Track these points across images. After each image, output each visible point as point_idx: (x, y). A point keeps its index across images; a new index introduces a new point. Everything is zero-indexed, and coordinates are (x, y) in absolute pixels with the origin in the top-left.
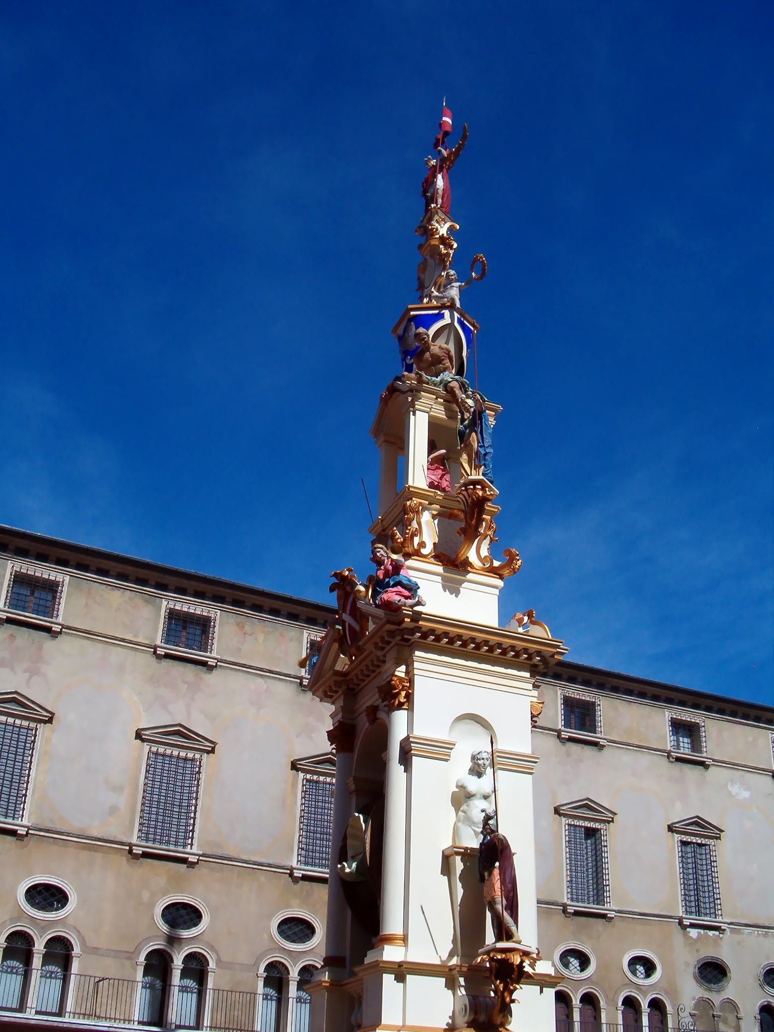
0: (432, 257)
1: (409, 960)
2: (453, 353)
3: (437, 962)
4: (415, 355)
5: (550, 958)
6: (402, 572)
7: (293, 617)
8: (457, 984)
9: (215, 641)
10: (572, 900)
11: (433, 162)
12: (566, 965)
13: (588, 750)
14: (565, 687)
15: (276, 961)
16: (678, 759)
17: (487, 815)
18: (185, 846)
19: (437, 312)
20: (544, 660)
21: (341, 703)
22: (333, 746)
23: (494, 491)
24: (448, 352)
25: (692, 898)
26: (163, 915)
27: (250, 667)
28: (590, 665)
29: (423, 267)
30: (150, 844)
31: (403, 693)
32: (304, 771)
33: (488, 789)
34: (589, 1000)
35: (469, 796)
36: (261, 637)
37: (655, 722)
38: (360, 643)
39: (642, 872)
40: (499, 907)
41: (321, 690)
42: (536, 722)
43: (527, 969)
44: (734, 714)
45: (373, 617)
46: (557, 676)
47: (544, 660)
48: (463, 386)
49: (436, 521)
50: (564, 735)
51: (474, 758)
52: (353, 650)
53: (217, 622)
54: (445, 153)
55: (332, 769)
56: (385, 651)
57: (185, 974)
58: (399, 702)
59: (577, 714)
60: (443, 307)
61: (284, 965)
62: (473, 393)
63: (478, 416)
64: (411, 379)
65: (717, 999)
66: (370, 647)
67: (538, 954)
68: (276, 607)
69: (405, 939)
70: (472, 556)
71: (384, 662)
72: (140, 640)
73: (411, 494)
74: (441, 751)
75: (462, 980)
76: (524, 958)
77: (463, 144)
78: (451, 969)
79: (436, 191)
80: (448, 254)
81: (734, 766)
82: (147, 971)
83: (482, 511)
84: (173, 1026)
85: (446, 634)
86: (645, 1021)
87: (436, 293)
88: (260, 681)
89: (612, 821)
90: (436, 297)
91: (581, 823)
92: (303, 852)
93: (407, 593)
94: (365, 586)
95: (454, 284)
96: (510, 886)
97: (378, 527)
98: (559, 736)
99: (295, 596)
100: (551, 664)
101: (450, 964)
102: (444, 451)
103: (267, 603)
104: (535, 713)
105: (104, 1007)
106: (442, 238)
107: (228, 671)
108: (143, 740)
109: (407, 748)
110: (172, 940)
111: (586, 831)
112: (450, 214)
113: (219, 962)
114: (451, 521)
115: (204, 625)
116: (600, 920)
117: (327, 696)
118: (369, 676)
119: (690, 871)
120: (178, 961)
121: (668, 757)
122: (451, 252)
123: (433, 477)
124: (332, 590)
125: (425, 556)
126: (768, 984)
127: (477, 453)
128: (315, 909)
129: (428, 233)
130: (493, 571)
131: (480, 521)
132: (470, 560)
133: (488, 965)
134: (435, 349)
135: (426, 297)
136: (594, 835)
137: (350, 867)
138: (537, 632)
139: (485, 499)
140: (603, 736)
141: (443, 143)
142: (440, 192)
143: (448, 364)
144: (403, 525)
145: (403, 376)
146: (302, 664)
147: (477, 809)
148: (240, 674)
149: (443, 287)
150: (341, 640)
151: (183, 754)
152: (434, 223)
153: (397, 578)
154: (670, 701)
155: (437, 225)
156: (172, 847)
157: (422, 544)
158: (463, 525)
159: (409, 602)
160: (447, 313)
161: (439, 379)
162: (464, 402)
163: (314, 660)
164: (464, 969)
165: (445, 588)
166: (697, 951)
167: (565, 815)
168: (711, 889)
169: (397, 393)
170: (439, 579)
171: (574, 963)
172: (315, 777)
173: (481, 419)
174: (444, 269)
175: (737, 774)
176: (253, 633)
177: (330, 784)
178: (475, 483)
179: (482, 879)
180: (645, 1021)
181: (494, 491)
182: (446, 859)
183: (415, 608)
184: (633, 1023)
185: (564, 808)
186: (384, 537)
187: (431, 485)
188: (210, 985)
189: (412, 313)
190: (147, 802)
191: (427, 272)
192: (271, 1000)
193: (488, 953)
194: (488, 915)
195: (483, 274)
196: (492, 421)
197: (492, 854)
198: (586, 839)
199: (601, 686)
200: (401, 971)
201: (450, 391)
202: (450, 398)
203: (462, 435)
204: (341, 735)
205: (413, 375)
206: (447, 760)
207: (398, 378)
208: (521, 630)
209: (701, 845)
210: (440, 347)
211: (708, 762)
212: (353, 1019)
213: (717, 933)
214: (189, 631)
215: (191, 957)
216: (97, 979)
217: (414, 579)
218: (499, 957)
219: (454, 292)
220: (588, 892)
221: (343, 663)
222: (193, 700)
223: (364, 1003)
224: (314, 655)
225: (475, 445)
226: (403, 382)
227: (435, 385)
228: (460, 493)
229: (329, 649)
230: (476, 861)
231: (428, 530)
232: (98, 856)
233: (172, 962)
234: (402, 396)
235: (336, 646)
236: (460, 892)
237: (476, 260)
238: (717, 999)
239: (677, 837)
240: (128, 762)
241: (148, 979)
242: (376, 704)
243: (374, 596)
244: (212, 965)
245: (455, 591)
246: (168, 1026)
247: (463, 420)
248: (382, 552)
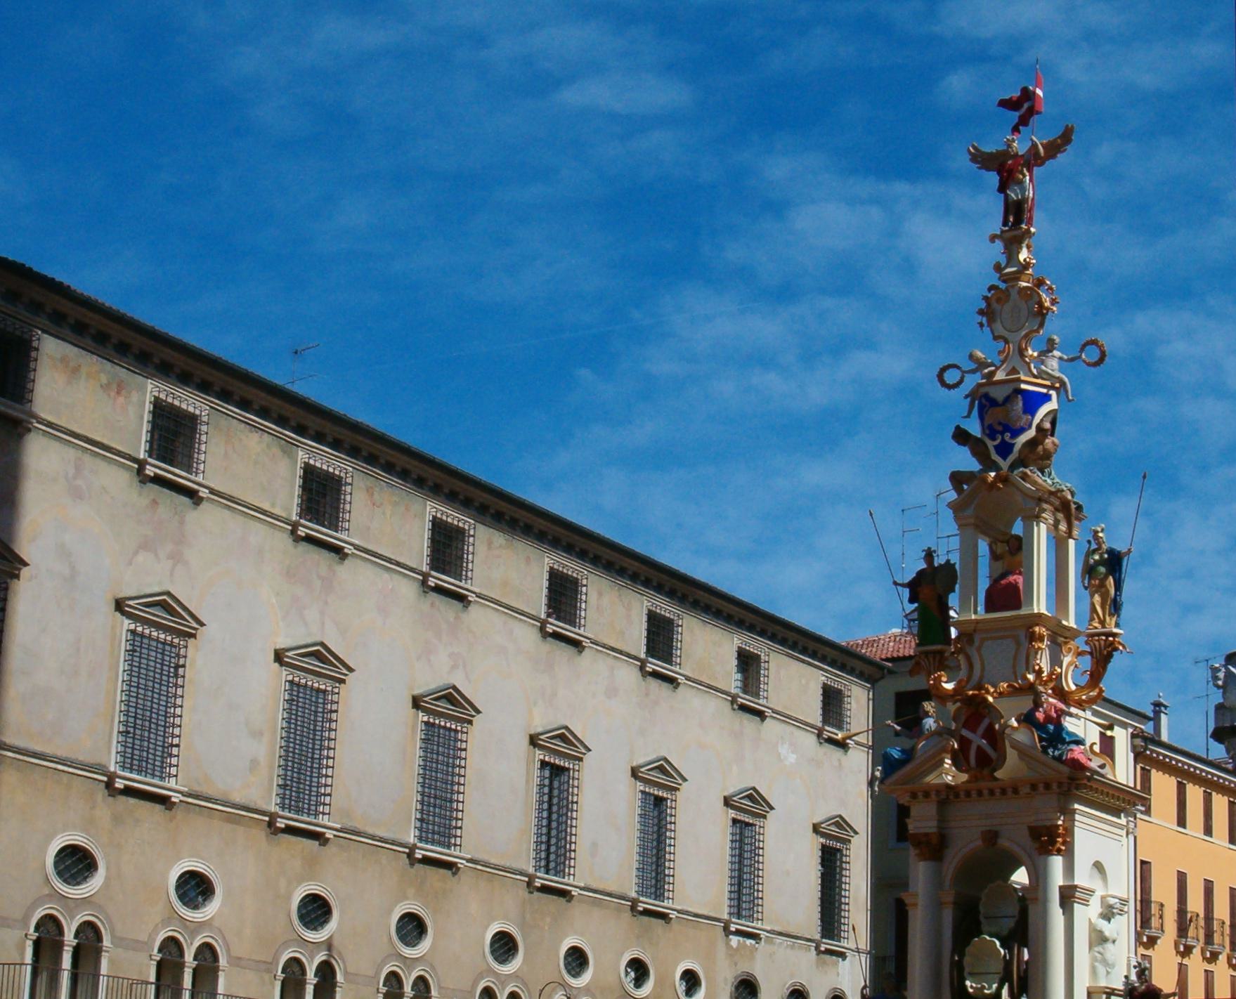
19: (1044, 391)
28: (244, 366)
72: (277, 511)
89: (194, 636)
121: (733, 702)
148: (369, 565)
167: (130, 616)
185: (131, 603)
209: (748, 824)
213: (753, 942)
222: (326, 603)
239: (732, 814)
240: (265, 690)
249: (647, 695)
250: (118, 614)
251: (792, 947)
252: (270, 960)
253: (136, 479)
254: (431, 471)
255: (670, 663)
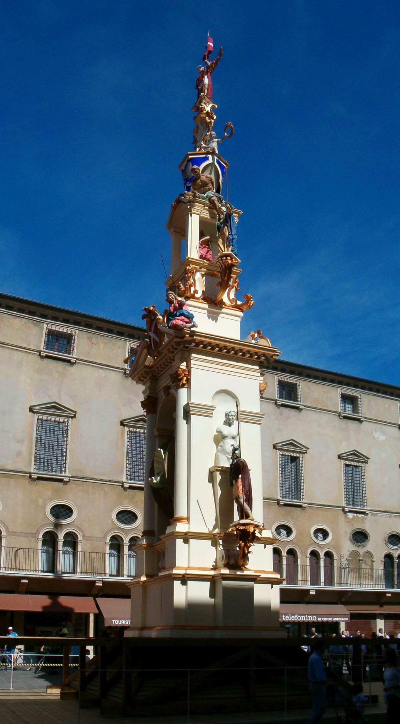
0: (201, 124)
1: (191, 531)
2: (214, 180)
3: (207, 531)
4: (192, 181)
5: (270, 529)
6: (184, 308)
7: (120, 334)
8: (218, 544)
9: (75, 348)
10: (283, 497)
11: (202, 69)
12: (279, 534)
13: (293, 412)
14: (279, 374)
15: (116, 535)
16: (345, 417)
17: (234, 448)
18: (61, 472)
19: (204, 156)
20: (267, 359)
21: (148, 384)
22: (145, 410)
23: (238, 260)
24: (211, 180)
25: (351, 496)
26: (51, 512)
27: (95, 363)
29: (197, 128)
30: (41, 472)
31: (185, 378)
32: (128, 426)
33: (235, 433)
34: (292, 552)
35: (224, 437)
36: (102, 346)
37: (332, 395)
38: (160, 349)
39: (322, 481)
40: (241, 500)
41: (137, 376)
42: (262, 394)
43: (257, 534)
44: (378, 391)
45: (167, 334)
46: (275, 369)
47: (267, 359)
48: (220, 200)
49: (204, 278)
50: (279, 403)
51: (227, 415)
52: (156, 353)
53: (76, 337)
54: (209, 63)
55: (145, 425)
56: (174, 354)
57: (65, 544)
58: (183, 383)
59: (286, 390)
60: (208, 153)
61: (120, 537)
62: (226, 203)
63: (229, 217)
64: (189, 195)
65: (362, 551)
66: (165, 351)
67: (263, 526)
68: (110, 328)
69: (188, 519)
70: (225, 298)
71: (174, 360)
72: (31, 347)
73: (189, 262)
74: (207, 411)
75: (221, 542)
76: (256, 528)
77: (220, 58)
78: (215, 535)
79: (204, 85)
80: (211, 122)
81: (377, 421)
82: (44, 543)
83: (230, 272)
84: (60, 573)
85: (210, 344)
86: (322, 563)
87: (204, 145)
88: (101, 371)
89: (306, 453)
90: (204, 147)
91: (288, 454)
92: (129, 473)
93: (187, 320)
94: (164, 317)
95: (214, 140)
96: (247, 488)
97: (170, 281)
98: (276, 403)
99: (122, 322)
100: (271, 362)
101: (214, 533)
102: (208, 237)
103: (105, 326)
104: (262, 389)
105: (21, 564)
106: (207, 113)
107: (83, 366)
108: (34, 412)
109: (188, 410)
110: (57, 526)
111: (291, 458)
112: (212, 99)
113: (84, 537)
114: (213, 278)
115: (68, 339)
116: (298, 509)
117: (140, 380)
118: (165, 368)
119: (350, 481)
120: (61, 537)
121: (339, 416)
122: (213, 121)
123: (202, 252)
124: (143, 318)
125: (198, 299)
126: (390, 543)
127: (228, 238)
128: (137, 504)
129: (200, 110)
130: (237, 307)
131: (229, 278)
132: (224, 301)
133: (235, 533)
134: (203, 177)
135: (198, 147)
136: (296, 460)
137: (156, 480)
138: (263, 342)
139: (232, 265)
140: (301, 403)
141: (208, 57)
142: (206, 86)
143: (211, 186)
144: (185, 280)
145: (185, 193)
146: (126, 361)
147: (229, 445)
148: (90, 367)
149: (208, 142)
150: (148, 347)
151: (57, 419)
152: (203, 104)
153: (181, 311)
154: (340, 383)
155: (204, 105)
156: (54, 473)
157: (196, 292)
158: (220, 280)
159: (188, 325)
160: (210, 157)
161: (205, 195)
162: (220, 208)
163: (133, 359)
164: (222, 535)
165: (209, 317)
166: (352, 525)
167: (279, 449)
168: (361, 491)
169: (181, 204)
170: (206, 312)
171: (284, 532)
172: (135, 430)
173: (230, 218)
174: (209, 131)
175: (379, 426)
176: (97, 343)
177: (143, 433)
178: (227, 256)
179: (232, 485)
180: (322, 563)
181: (238, 260)
182: (211, 474)
183: (192, 329)
184: (315, 564)
186: (173, 287)
187: (201, 257)
188: (80, 549)
189: (190, 157)
190: (38, 449)
191: (199, 133)
192: (114, 556)
193: (235, 526)
194: (236, 505)
195: (231, 134)
196: (236, 220)
197: (237, 470)
198: (291, 463)
199: (300, 374)
200: (186, 537)
201: (212, 202)
202: (212, 206)
203: (219, 228)
204: (149, 404)
205: (190, 193)
206: (211, 417)
207: (182, 195)
208: (253, 342)
209: (356, 466)
210: (206, 177)
211: (362, 419)
212: (160, 565)
213: (363, 515)
214: (59, 342)
215: (68, 535)
216: (16, 549)
217: (191, 312)
218: (242, 528)
219: (214, 144)
220: (292, 489)
221: (149, 360)
223: (166, 555)
224: (133, 356)
225: (227, 234)
226: (185, 197)
227: (203, 199)
228: (218, 262)
229: (141, 353)
230: (228, 474)
231: (199, 283)
232: (12, 481)
233: (58, 537)
234: (184, 205)
235: (145, 351)
236: (219, 492)
237: (227, 126)
238: (362, 551)
239: (343, 462)
241: (45, 548)
242: (169, 385)
243: (168, 322)
244: (80, 538)
245: (215, 319)
246: (58, 573)
247: (220, 219)
248: (172, 296)
249: (281, 414)
250: (274, 450)
251: (390, 517)
252: (34, 532)
253: (275, 406)
254: (136, 331)
255: (297, 401)
